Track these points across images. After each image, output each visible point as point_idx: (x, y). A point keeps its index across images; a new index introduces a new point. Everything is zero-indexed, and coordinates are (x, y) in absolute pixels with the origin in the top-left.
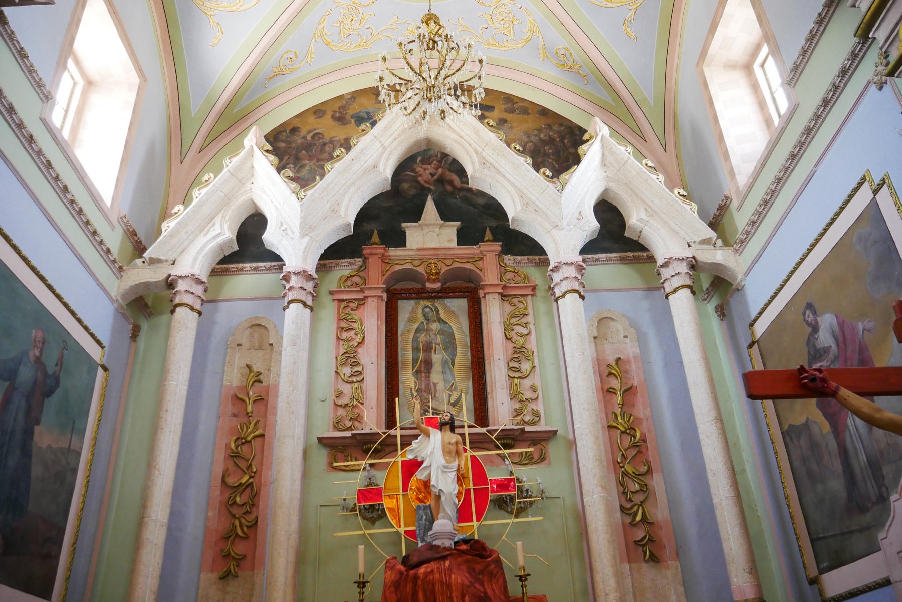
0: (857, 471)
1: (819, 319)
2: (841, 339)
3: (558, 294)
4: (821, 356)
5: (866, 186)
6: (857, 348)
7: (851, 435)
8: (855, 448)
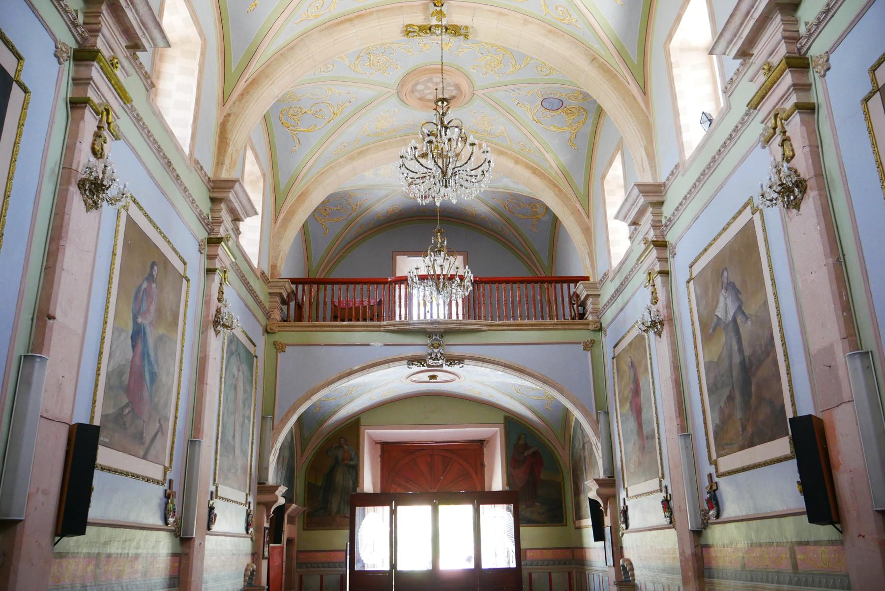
5: (749, 208)
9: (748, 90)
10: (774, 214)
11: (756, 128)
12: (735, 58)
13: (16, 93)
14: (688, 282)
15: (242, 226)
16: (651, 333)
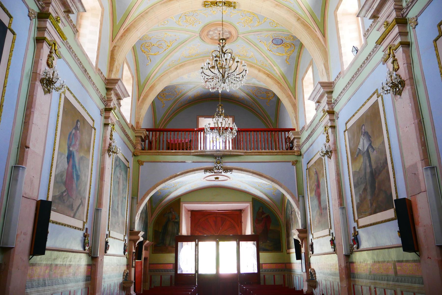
9: (376, 35)
10: (388, 98)
11: (380, 54)
12: (370, 19)
13: (9, 35)
14: (345, 132)
15: (122, 102)
16: (326, 157)
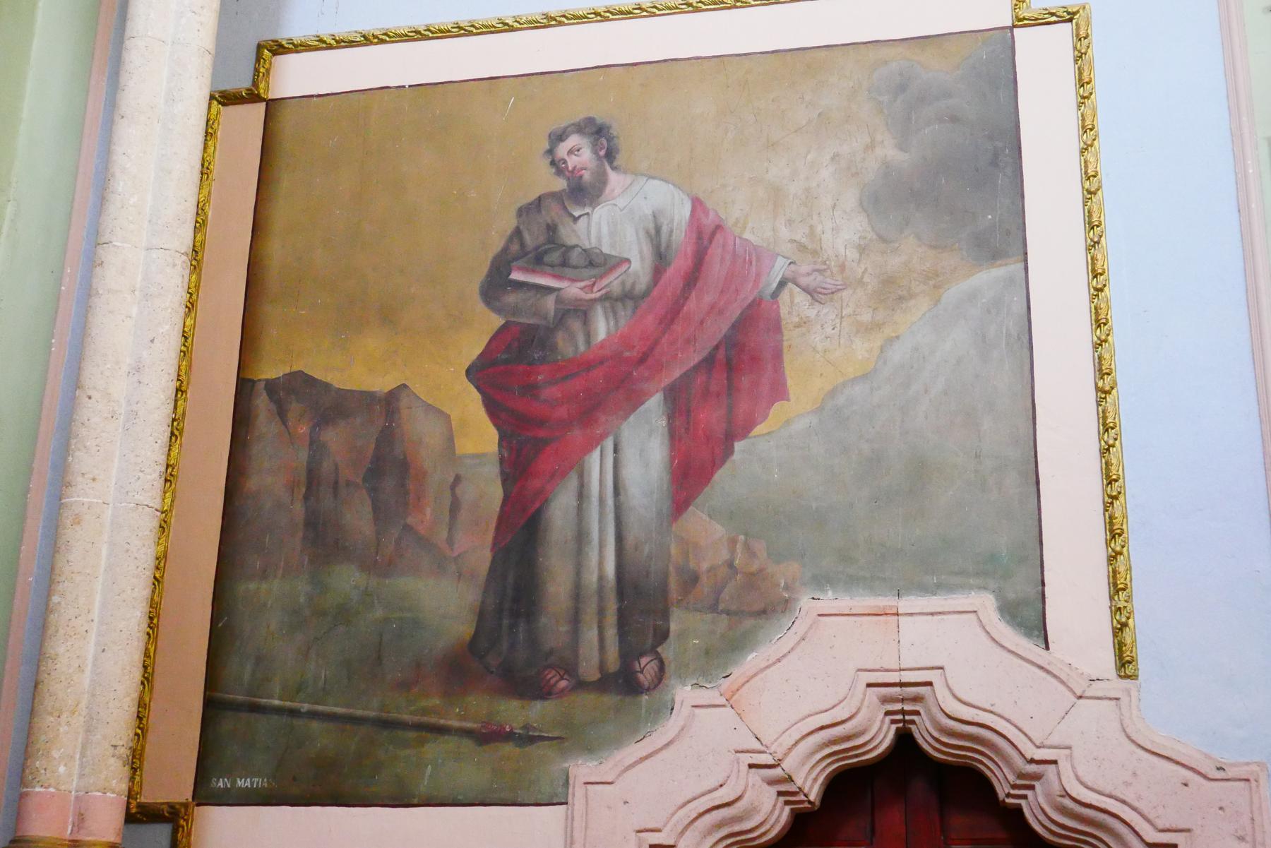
0: (557, 587)
1: (613, 176)
2: (679, 265)
3: (560, 184)
4: (565, 263)
6: (734, 313)
7: (582, 495)
8: (581, 537)
